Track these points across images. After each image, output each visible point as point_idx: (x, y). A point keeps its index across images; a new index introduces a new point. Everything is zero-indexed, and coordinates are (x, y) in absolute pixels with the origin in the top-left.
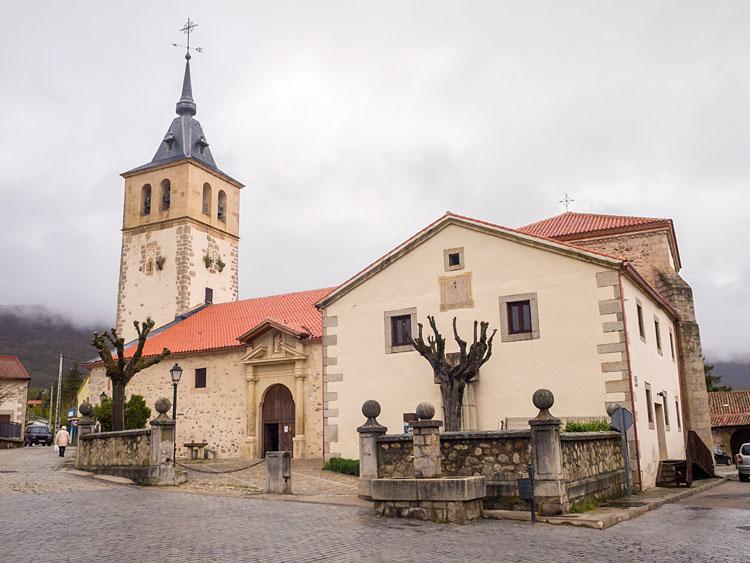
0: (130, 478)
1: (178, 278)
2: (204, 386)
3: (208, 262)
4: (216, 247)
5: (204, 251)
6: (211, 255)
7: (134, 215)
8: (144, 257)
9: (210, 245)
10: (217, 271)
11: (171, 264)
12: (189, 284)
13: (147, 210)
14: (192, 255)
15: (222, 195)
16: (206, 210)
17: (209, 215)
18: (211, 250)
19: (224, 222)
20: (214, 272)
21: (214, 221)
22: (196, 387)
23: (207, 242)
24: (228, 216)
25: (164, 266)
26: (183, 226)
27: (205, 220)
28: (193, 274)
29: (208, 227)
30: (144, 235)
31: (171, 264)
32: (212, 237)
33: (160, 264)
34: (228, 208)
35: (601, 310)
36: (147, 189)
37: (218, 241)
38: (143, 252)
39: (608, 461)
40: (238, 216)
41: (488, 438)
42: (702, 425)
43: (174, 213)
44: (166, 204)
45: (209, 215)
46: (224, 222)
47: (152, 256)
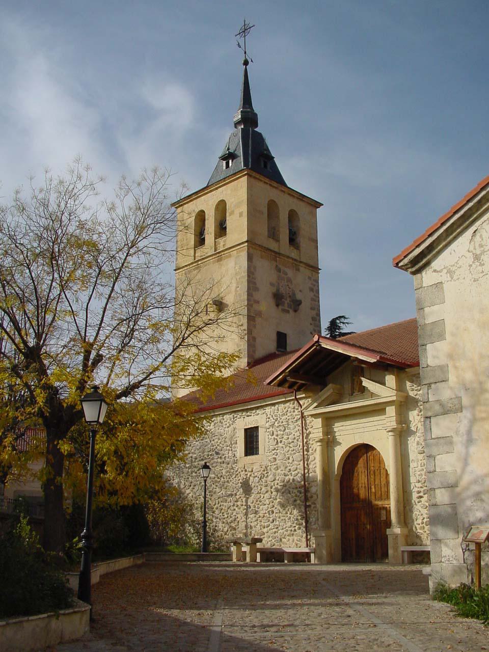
0: (255, 644)
2: (246, 430)
3: (278, 298)
4: (289, 280)
6: (282, 290)
10: (291, 311)
15: (292, 215)
17: (277, 240)
19: (297, 248)
20: (288, 312)
21: (284, 246)
22: (246, 455)
24: (303, 241)
27: (273, 245)
35: (252, 454)
36: (201, 217)
39: (270, 512)
40: (316, 241)
42: (451, 543)
45: (277, 240)
46: (297, 248)
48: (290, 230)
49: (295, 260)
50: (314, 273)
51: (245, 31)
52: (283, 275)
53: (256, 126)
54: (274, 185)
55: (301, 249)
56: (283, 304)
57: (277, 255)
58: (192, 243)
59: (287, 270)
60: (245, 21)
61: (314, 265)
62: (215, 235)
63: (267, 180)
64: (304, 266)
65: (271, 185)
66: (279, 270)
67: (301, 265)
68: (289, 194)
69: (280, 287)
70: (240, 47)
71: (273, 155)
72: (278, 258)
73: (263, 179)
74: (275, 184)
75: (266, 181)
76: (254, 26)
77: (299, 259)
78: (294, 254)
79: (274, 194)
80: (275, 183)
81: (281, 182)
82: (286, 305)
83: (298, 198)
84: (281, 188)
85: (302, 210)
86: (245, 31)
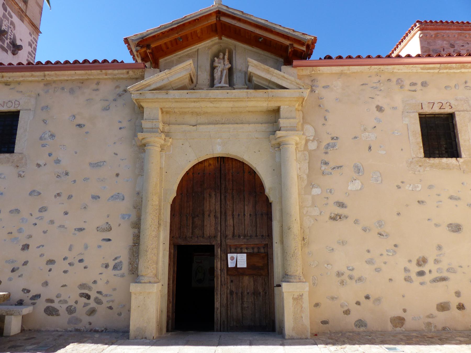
37: (15, 19)
49: (22, 11)
50: (35, 33)
59: (13, 14)
64: (28, 20)
69: (3, 25)
77: (24, 11)
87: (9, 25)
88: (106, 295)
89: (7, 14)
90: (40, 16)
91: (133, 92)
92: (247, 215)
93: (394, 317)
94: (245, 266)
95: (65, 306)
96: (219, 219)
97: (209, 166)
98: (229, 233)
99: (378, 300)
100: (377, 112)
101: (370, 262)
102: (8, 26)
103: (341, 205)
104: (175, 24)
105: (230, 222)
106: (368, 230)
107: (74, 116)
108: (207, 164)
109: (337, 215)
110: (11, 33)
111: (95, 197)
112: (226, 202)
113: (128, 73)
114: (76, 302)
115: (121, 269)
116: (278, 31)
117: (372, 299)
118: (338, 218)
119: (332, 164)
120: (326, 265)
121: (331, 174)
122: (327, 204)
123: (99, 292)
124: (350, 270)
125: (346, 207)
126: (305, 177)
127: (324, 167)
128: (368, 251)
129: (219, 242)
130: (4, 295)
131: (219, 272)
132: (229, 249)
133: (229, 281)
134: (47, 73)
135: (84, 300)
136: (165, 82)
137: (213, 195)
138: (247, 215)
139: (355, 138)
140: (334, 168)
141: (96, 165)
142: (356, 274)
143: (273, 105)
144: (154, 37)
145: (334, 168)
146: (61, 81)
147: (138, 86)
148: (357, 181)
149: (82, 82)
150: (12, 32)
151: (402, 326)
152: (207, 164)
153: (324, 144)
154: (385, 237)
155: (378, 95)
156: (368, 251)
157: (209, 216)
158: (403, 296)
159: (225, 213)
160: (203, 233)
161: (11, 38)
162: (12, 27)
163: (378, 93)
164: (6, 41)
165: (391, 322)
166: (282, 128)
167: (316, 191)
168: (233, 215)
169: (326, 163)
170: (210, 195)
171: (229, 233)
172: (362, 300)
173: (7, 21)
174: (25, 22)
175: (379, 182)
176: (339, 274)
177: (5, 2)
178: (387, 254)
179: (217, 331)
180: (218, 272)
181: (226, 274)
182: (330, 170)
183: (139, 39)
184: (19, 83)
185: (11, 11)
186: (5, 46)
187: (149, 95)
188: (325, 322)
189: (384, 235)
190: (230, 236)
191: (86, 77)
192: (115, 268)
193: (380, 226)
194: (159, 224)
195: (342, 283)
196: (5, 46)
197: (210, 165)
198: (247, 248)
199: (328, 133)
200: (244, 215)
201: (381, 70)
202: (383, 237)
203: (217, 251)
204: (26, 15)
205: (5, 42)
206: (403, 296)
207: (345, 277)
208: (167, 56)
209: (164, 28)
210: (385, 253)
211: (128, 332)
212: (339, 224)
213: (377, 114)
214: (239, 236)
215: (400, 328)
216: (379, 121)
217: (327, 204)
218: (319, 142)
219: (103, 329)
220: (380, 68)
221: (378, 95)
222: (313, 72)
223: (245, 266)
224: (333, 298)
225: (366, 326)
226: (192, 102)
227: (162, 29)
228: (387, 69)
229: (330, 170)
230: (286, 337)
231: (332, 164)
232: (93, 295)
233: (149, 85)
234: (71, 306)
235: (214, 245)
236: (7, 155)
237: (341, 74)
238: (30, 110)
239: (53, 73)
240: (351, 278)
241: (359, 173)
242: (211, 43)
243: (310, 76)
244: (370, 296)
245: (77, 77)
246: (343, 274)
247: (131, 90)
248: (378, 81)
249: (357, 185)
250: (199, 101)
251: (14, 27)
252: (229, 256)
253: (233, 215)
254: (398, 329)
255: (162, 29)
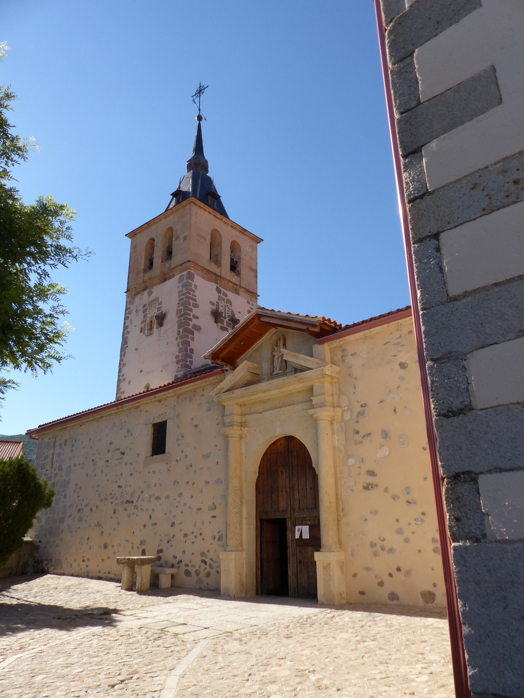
1: (179, 333)
2: (154, 425)
4: (229, 301)
5: (212, 303)
6: (221, 309)
7: (138, 273)
8: (145, 316)
9: (220, 298)
11: (172, 320)
12: (193, 339)
13: (151, 264)
14: (196, 306)
15: (234, 247)
16: (215, 258)
18: (222, 303)
19: (238, 274)
21: (225, 270)
23: (217, 294)
24: (243, 269)
25: (165, 321)
26: (185, 273)
27: (213, 268)
28: (198, 328)
29: (216, 278)
30: (146, 293)
31: (172, 320)
32: (222, 290)
33: (161, 319)
34: (243, 262)
37: (231, 296)
38: (145, 311)
40: (256, 271)
41: (234, 551)
43: (177, 259)
44: (169, 253)
47: (153, 312)
48: (232, 260)
49: (236, 285)
50: (253, 298)
51: (200, 91)
52: (223, 297)
53: (207, 172)
54: (218, 216)
55: (241, 276)
56: (222, 322)
57: (218, 278)
58: (142, 267)
59: (227, 292)
60: (200, 83)
61: (253, 291)
62: (163, 259)
63: (211, 210)
64: (243, 290)
65: (215, 216)
66: (219, 291)
67: (242, 290)
68: (232, 227)
69: (220, 306)
70: (195, 103)
71: (219, 194)
72: (219, 281)
73: (207, 209)
74: (219, 216)
75: (210, 211)
76: (208, 86)
77: (238, 284)
78: (234, 279)
79: (218, 224)
80: (219, 214)
81: (221, 211)
82: (225, 324)
83: (240, 232)
84: (224, 220)
85: (244, 243)
86: (200, 91)
87: (225, 304)
88: (215, 562)
89: (221, 295)
90: (256, 280)
91: (214, 397)
92: (308, 488)
93: (424, 591)
94: (308, 537)
95: (194, 569)
96: (289, 494)
97: (280, 445)
98: (296, 506)
99: (408, 573)
100: (401, 370)
101: (399, 532)
102: (225, 305)
103: (372, 473)
104: (231, 335)
105: (297, 496)
106: (397, 498)
107: (192, 419)
108: (279, 444)
109: (369, 484)
110: (228, 311)
111: (207, 483)
112: (293, 478)
113: (217, 378)
114: (200, 567)
115: (222, 541)
116: (296, 320)
117: (403, 571)
118: (370, 487)
119: (362, 433)
120: (361, 536)
121: (362, 442)
122: (359, 474)
123: (211, 559)
124: (381, 540)
125: (376, 475)
126: (343, 448)
127: (356, 437)
128: (397, 521)
129: (289, 515)
130: (152, 558)
131: (291, 542)
132: (297, 521)
133: (298, 552)
134: (175, 389)
135: (203, 565)
136: (232, 383)
137: (284, 472)
138: (308, 488)
139: (381, 402)
140: (364, 436)
141: (206, 456)
142: (387, 545)
143: (308, 384)
144: (220, 349)
145: (364, 436)
146: (185, 393)
147: (216, 391)
148: (385, 447)
149: (195, 390)
150: (230, 309)
151: (433, 601)
152: (279, 444)
153: (355, 413)
154: (413, 505)
155: (401, 351)
156: (397, 521)
157: (282, 491)
158: (433, 569)
159: (293, 488)
160: (278, 508)
161: (229, 316)
162: (229, 305)
163: (401, 349)
164: (225, 321)
165: (422, 596)
166: (315, 406)
167: (351, 461)
168: (299, 490)
169: (357, 432)
170: (282, 472)
171: (296, 506)
172: (394, 572)
173: (223, 302)
174: (241, 293)
175: (405, 446)
176: (373, 545)
177: (218, 286)
178: (416, 524)
179: (292, 597)
180: (289, 543)
181: (295, 545)
182: (361, 439)
183: (211, 354)
184: (165, 399)
185: (225, 291)
186: (225, 325)
187: (223, 397)
188: (362, 593)
189: (412, 502)
190: (297, 509)
191: (196, 387)
192: (219, 539)
193: (408, 493)
194: (241, 502)
195: (375, 554)
196: (225, 325)
197: (281, 444)
198: (310, 521)
199: (358, 402)
200: (306, 489)
201: (399, 324)
202: (411, 505)
203: (288, 524)
204: (240, 287)
205: (223, 321)
206: (433, 569)
207: (378, 548)
208: (241, 356)
209: (225, 340)
210: (413, 522)
211: (220, 591)
212: (372, 493)
213: (402, 372)
214: (303, 510)
215: (432, 603)
216: (402, 378)
217: (359, 474)
218: (352, 411)
219: (214, 589)
220: (398, 323)
221: (401, 351)
222: (341, 343)
223: (308, 537)
224: (368, 569)
225: (398, 599)
226: (251, 395)
227: (224, 342)
228: (405, 321)
229: (361, 439)
230: (319, 603)
231: (362, 433)
232: (208, 561)
233: (223, 388)
234: (197, 570)
235: (285, 520)
236: (162, 455)
237: (366, 338)
238: (172, 418)
239: (178, 388)
240: (383, 548)
241: (386, 439)
242: (271, 335)
243: (340, 347)
244: (401, 568)
245: (192, 388)
246: (375, 545)
247: (213, 395)
248: (399, 336)
249: (384, 452)
250: (255, 394)
251: (231, 304)
252: (297, 527)
253: (299, 490)
254: (430, 605)
255: (224, 342)
